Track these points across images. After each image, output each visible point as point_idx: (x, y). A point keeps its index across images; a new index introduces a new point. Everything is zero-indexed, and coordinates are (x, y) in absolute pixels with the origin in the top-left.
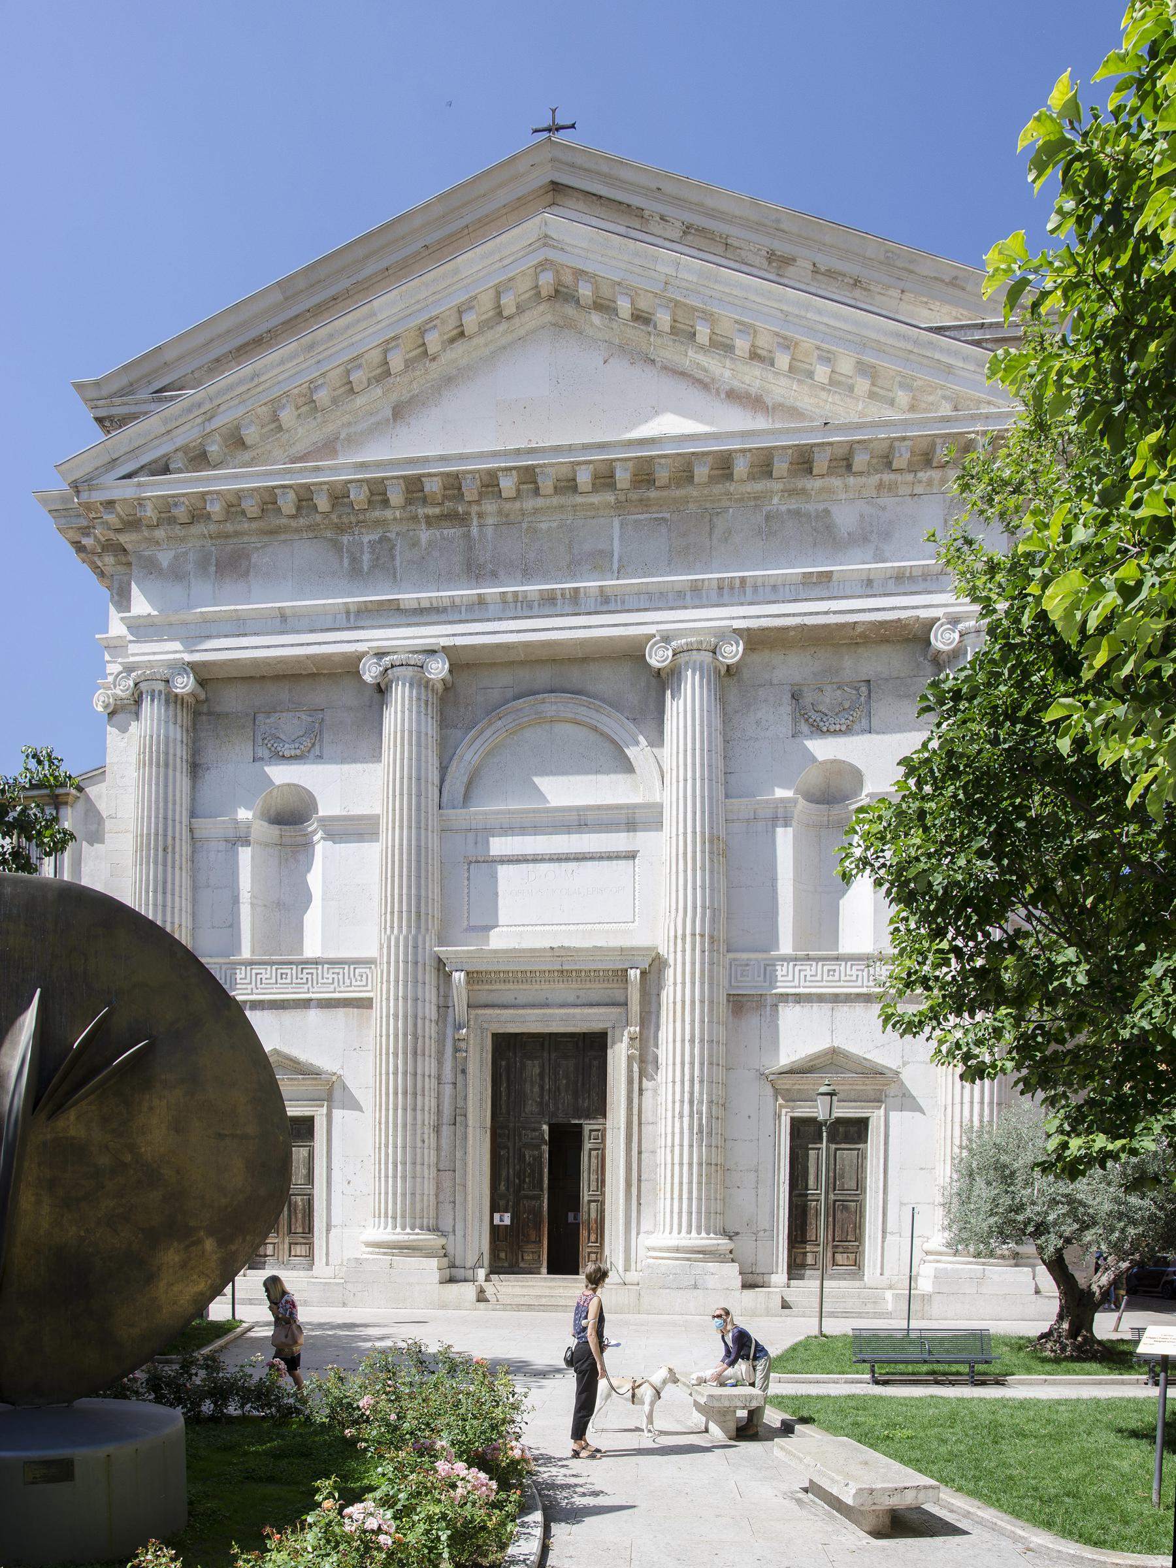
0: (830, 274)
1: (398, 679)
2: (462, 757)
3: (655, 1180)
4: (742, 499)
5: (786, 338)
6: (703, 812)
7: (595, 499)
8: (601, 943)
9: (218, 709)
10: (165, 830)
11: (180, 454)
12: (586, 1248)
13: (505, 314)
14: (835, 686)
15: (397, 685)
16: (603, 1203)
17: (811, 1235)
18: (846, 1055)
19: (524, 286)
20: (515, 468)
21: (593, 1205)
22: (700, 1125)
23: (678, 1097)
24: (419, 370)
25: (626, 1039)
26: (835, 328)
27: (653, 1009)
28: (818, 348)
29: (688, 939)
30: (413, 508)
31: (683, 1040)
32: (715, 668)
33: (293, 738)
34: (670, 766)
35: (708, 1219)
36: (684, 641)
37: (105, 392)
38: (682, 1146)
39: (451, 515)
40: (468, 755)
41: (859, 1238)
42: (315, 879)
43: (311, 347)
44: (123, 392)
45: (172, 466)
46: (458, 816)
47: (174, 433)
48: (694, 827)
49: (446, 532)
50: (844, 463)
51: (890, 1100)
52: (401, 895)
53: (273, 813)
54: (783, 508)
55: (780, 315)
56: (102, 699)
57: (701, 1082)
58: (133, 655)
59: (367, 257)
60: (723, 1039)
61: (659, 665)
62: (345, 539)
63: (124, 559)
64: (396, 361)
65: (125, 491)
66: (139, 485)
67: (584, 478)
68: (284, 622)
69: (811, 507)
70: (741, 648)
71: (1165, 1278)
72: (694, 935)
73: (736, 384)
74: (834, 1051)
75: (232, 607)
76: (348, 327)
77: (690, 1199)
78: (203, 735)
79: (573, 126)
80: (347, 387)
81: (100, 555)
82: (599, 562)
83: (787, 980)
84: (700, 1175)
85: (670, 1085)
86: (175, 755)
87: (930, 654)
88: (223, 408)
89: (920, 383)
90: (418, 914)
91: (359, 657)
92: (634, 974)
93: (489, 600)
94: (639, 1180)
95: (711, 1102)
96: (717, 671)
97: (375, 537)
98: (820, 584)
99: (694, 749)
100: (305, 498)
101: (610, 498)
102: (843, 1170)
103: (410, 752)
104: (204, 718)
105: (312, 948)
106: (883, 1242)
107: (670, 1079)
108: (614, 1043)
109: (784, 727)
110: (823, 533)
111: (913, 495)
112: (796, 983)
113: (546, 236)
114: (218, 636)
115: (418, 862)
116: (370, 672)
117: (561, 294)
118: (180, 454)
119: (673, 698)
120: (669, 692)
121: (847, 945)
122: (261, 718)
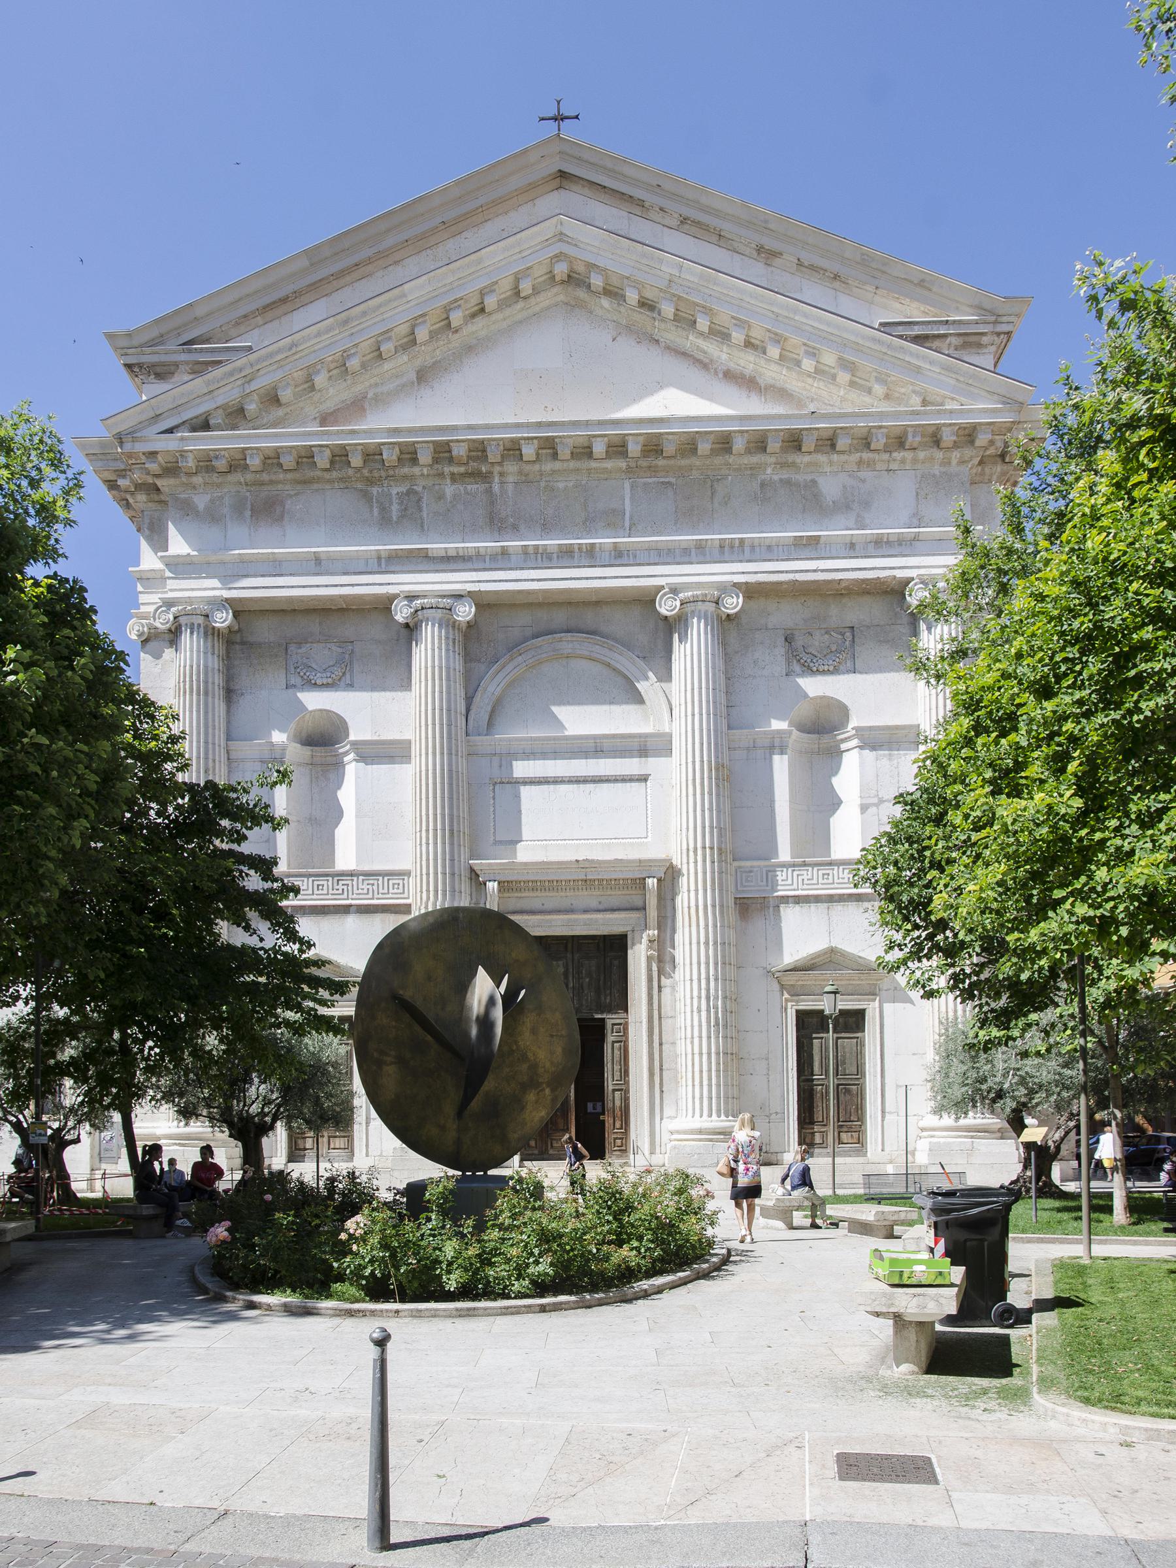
0: (813, 268)
1: (427, 620)
2: (485, 689)
3: (676, 1070)
4: (739, 469)
5: (776, 334)
6: (709, 744)
7: (609, 464)
8: (620, 855)
9: (251, 639)
10: (206, 753)
11: (220, 411)
12: (611, 1135)
13: (522, 295)
14: (823, 631)
15: (427, 625)
16: (627, 1091)
17: (818, 1116)
18: (843, 954)
19: (539, 272)
20: (536, 438)
21: (617, 1094)
22: (717, 1018)
23: (695, 993)
24: (444, 341)
25: (645, 940)
26: (820, 330)
27: (669, 914)
28: (805, 344)
29: (700, 852)
30: (440, 467)
31: (699, 943)
32: (718, 615)
33: (324, 667)
34: (679, 697)
35: (726, 1103)
36: (690, 594)
37: (135, 343)
38: (700, 1037)
39: (476, 477)
40: (492, 687)
41: (861, 1118)
42: (347, 795)
43: (346, 322)
44: (152, 343)
45: (212, 422)
46: (483, 742)
47: (215, 393)
48: (702, 757)
49: (469, 487)
50: (829, 443)
51: (883, 993)
52: (435, 815)
53: (304, 735)
54: (776, 478)
55: (771, 315)
56: (136, 628)
57: (716, 979)
58: (171, 590)
59: (389, 230)
60: (733, 941)
61: (668, 614)
62: (375, 490)
63: (156, 498)
64: (422, 334)
65: (169, 444)
66: (182, 439)
67: (599, 448)
68: (319, 565)
69: (799, 478)
70: (741, 600)
71: (1157, 1155)
72: (704, 848)
73: (732, 365)
74: (832, 951)
75: (270, 551)
76: (380, 306)
77: (710, 1085)
78: (236, 663)
79: (577, 117)
80: (376, 353)
81: (132, 493)
82: (613, 520)
83: (787, 883)
84: (718, 1064)
85: (688, 983)
86: (213, 683)
88: (261, 372)
89: (893, 379)
90: (452, 831)
91: (391, 598)
92: (652, 883)
93: (511, 551)
94: (661, 1070)
95: (725, 998)
96: (719, 618)
97: (403, 489)
98: (810, 546)
99: (700, 688)
100: (340, 456)
101: (622, 464)
102: (844, 1056)
103: (441, 686)
104: (238, 647)
105: (346, 857)
106: (883, 1121)
107: (688, 977)
108: (633, 944)
109: (780, 667)
110: (811, 501)
111: (888, 471)
112: (795, 886)
113: (561, 233)
114: (255, 576)
115: (451, 784)
117: (573, 280)
118: (220, 411)
119: (680, 641)
120: (676, 636)
122: (292, 648)
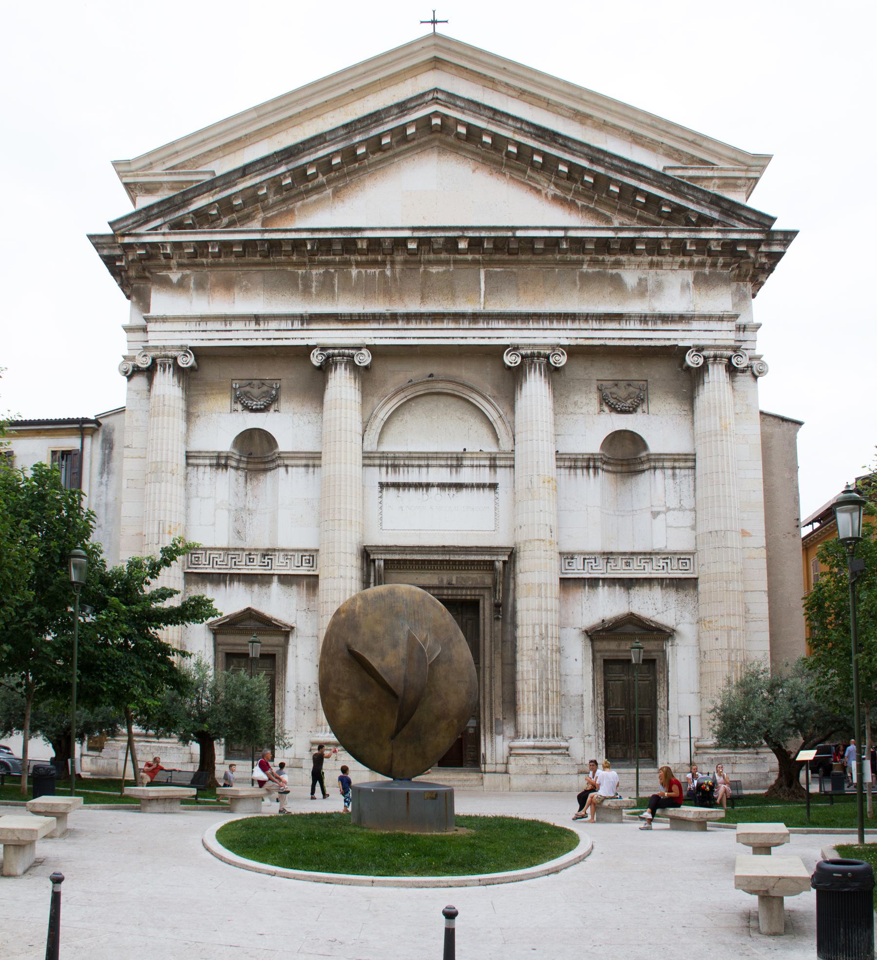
49: (369, 271)
91: (309, 348)
121: (78, 447)
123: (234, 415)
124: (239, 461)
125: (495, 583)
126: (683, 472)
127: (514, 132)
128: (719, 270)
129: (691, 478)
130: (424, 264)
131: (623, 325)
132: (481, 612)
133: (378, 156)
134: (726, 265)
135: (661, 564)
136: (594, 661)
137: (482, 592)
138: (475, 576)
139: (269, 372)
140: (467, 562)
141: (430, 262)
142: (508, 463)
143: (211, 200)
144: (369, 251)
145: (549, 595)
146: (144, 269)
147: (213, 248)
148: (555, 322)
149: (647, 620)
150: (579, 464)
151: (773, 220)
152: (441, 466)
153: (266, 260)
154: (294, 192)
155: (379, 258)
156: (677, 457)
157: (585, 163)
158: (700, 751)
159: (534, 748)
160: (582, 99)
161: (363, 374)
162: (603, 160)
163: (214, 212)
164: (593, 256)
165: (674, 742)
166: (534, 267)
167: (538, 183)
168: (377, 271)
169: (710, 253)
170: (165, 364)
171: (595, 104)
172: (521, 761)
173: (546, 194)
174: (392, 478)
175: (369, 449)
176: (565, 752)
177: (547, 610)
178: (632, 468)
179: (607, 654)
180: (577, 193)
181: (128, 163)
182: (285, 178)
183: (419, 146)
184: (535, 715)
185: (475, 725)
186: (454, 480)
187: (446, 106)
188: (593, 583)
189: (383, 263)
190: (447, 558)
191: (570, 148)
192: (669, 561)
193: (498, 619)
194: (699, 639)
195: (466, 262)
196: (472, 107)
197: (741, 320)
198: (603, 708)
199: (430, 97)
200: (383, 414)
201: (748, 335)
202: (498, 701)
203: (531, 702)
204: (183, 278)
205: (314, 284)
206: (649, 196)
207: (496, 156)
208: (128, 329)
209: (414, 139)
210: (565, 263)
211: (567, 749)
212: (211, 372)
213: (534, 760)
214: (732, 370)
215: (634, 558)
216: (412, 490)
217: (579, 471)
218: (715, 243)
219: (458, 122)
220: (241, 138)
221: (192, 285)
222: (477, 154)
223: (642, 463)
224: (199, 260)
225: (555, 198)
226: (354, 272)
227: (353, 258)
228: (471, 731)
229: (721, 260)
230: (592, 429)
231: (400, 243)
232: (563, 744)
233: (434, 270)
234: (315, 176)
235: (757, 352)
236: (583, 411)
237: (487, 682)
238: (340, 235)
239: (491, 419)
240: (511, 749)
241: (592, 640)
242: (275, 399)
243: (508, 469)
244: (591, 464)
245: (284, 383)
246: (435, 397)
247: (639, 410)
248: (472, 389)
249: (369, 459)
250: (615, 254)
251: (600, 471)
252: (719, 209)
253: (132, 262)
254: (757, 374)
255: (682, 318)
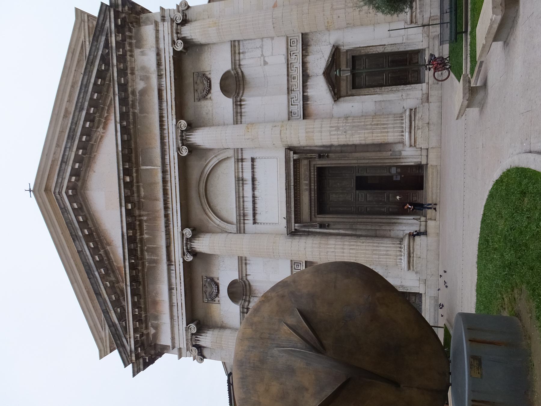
87: (184, 51)
91: (184, 262)
116: (180, 47)
123: (221, 302)
124: (245, 301)
125: (307, 158)
126: (241, 47)
127: (72, 151)
128: (133, 34)
129: (244, 42)
130: (140, 199)
131: (164, 88)
132: (324, 166)
133: (90, 222)
134: (130, 31)
135: (294, 57)
136: (353, 95)
137: (312, 166)
138: (303, 170)
139: (199, 283)
140: (295, 175)
141: (139, 196)
142: (240, 151)
143: (113, 311)
144: (134, 229)
145: (312, 126)
146: (151, 346)
147: (136, 312)
148: (164, 127)
149: (327, 63)
150: (239, 111)
151: (102, 4)
152: (243, 189)
153: (142, 283)
154: (109, 267)
155: (138, 223)
156: (233, 52)
157: (84, 113)
158: (414, 20)
159: (410, 132)
160: (58, 114)
161: (197, 232)
162: (81, 103)
163: (119, 310)
164: (130, 107)
165: (407, 39)
166: (138, 140)
167: (98, 138)
168: (145, 224)
169: (124, 40)
170: (196, 340)
171: (59, 107)
172: (419, 141)
173: (103, 133)
174: (250, 217)
175: (236, 229)
176: (413, 112)
177: (321, 127)
178: (241, 79)
179: (349, 87)
180: (101, 116)
181: (100, 351)
182: (101, 272)
183: (84, 201)
184: (388, 132)
185: (395, 168)
186: (250, 182)
187: (62, 187)
188: (305, 99)
189: (141, 221)
190: (292, 187)
191: (77, 121)
192: (292, 53)
193: (328, 156)
194: (339, 29)
195: (137, 176)
196: (61, 174)
197: (159, 19)
198: (383, 88)
199: (58, 196)
200: (218, 221)
201: (167, 14)
202: (379, 154)
203: (379, 135)
204: (153, 327)
205: (153, 258)
206: (97, 77)
207: (86, 160)
208: (180, 357)
209: (81, 204)
210: (135, 122)
211: (411, 110)
212: (200, 313)
213: (419, 133)
214: (185, 22)
215: (290, 74)
216: (257, 206)
217: (243, 110)
218: (118, 38)
219: (69, 181)
220: (87, 291)
221: (156, 322)
222: (86, 170)
223: (237, 73)
224: (143, 318)
225: (104, 128)
226: (146, 236)
227: (138, 237)
228: (399, 170)
229: (127, 33)
230: (220, 104)
231: (129, 213)
232: (408, 113)
233: (142, 194)
234: (100, 256)
235: (175, 8)
236: (210, 109)
237: (367, 161)
238: (126, 245)
239: (217, 162)
240: (411, 146)
241: (340, 97)
242: (212, 279)
243: (243, 152)
244: (239, 103)
245: (204, 274)
246: (208, 192)
247: (209, 76)
248: (202, 172)
249: (241, 230)
250: (128, 94)
251: (243, 98)
252: (100, 37)
253: (143, 353)
254: (186, 7)
255: (158, 54)
